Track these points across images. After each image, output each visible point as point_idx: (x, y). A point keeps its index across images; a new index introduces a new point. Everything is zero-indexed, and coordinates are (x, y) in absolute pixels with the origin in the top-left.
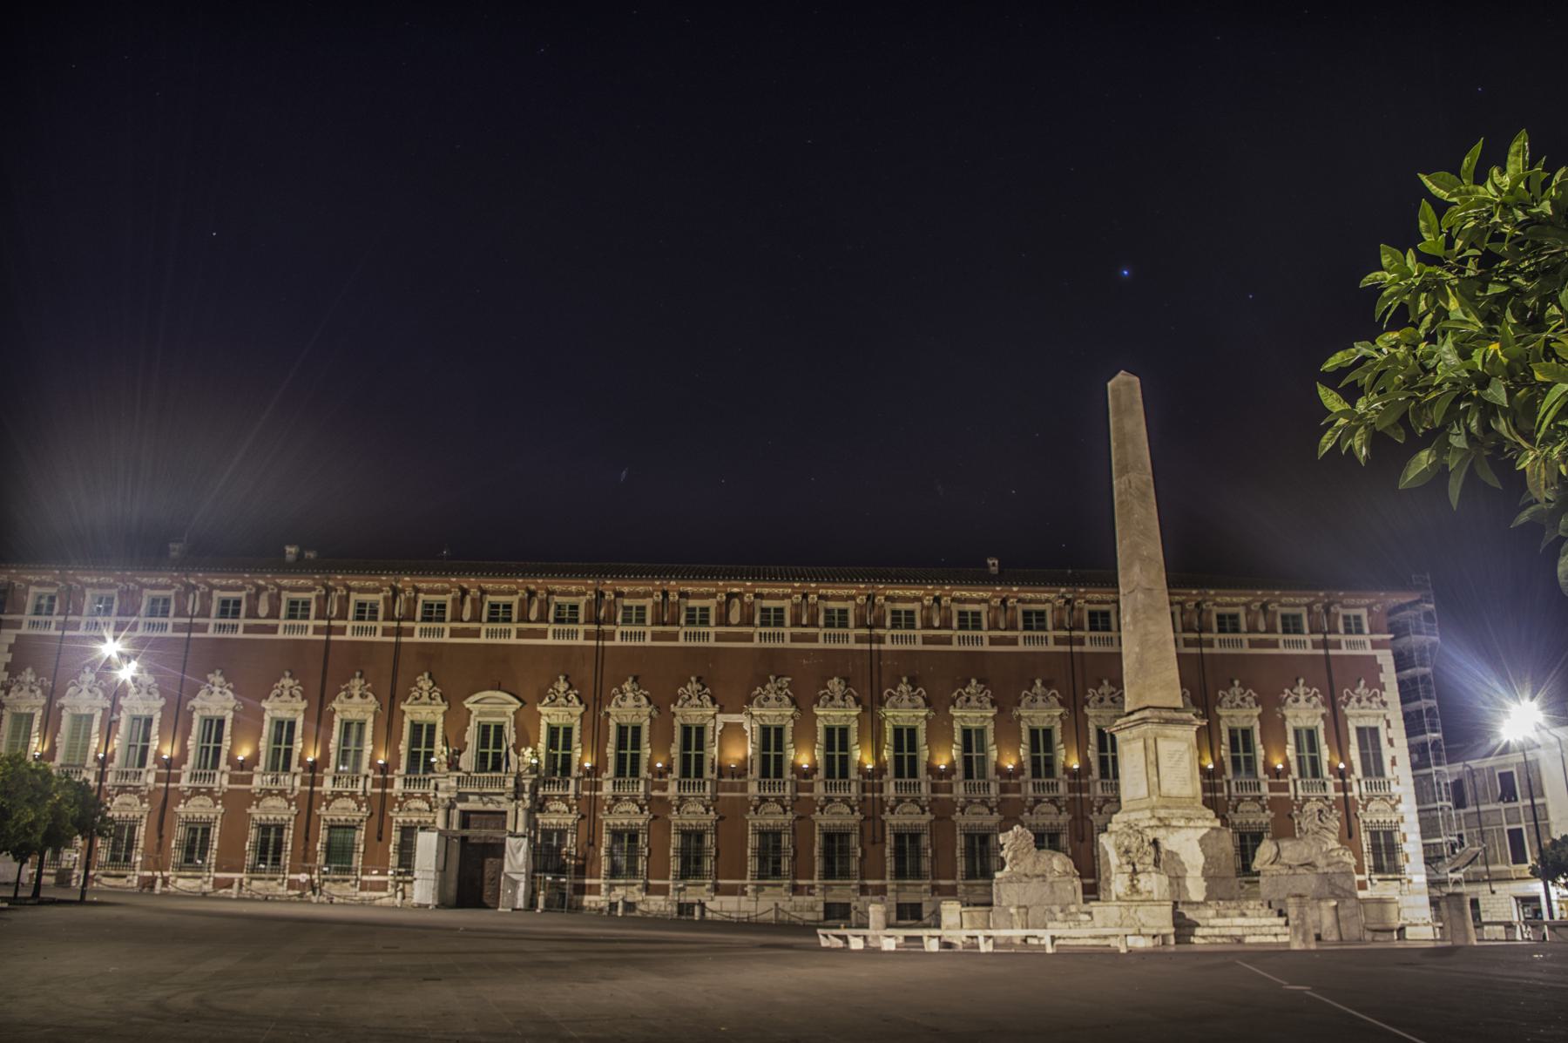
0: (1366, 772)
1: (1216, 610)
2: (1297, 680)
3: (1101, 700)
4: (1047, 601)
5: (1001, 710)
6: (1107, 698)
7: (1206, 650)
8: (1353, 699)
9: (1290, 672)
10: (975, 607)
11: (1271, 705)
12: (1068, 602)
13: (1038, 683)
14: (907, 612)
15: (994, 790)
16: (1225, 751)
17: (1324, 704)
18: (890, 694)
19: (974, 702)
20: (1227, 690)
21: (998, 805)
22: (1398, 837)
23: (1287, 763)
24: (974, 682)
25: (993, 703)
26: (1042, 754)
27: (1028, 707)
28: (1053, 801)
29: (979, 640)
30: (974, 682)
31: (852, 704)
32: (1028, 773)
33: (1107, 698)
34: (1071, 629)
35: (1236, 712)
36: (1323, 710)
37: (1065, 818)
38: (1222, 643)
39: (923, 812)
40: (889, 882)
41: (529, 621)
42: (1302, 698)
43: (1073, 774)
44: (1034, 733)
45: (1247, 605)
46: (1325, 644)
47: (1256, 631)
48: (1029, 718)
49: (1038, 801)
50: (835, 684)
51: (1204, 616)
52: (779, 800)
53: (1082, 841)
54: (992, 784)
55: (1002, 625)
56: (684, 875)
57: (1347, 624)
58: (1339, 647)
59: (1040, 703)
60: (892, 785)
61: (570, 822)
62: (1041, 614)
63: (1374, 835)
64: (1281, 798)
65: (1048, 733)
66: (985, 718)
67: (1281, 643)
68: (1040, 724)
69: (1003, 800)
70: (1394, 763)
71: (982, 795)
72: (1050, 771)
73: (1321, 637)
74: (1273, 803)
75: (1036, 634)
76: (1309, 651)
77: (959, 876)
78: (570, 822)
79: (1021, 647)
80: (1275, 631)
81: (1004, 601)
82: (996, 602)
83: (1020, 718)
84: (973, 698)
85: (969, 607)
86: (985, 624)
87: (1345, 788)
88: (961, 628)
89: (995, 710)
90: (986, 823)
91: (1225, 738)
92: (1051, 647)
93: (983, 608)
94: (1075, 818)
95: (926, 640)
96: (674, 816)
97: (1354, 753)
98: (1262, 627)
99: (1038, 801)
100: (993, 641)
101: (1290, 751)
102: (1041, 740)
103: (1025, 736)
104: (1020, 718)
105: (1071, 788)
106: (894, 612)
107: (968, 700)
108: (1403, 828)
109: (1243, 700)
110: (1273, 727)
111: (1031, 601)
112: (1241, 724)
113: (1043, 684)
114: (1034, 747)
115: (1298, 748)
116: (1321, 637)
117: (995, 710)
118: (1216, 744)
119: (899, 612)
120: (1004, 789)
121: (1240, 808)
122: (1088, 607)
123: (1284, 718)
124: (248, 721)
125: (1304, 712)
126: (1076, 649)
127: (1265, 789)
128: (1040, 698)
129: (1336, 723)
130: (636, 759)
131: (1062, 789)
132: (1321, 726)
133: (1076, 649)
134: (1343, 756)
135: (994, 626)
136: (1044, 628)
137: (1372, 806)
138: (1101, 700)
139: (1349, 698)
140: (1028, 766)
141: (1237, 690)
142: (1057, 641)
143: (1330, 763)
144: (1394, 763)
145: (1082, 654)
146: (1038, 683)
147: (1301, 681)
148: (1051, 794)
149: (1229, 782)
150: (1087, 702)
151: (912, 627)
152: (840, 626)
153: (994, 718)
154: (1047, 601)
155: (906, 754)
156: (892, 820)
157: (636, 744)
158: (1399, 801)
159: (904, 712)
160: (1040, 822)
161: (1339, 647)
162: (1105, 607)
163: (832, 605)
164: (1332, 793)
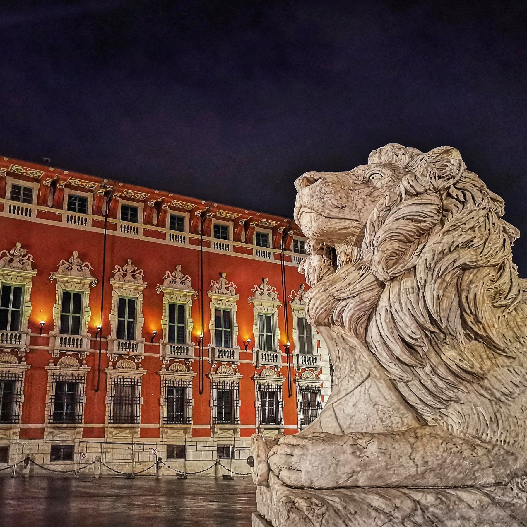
0: (302, 351)
1: (214, 221)
2: (263, 279)
3: (125, 275)
4: (90, 191)
5: (39, 273)
6: (129, 274)
7: (205, 249)
8: (298, 297)
9: (259, 272)
10: (28, 184)
11: (245, 294)
12: (107, 193)
13: (76, 254)
14: (26, 189)
15: (25, 341)
16: (212, 326)
17: (279, 299)
18: (63, 263)
19: (16, 263)
20: (216, 280)
21: (26, 356)
22: (319, 398)
23: (253, 338)
24: (19, 245)
25: (34, 266)
26: (176, 325)
27: (63, 273)
28: (76, 354)
29: (27, 212)
30: (19, 245)
31: (29, 268)
32: (57, 329)
33: (129, 274)
34: (107, 216)
35: (222, 297)
36: (278, 303)
37: (85, 370)
38: (216, 245)
39: (20, 360)
40: (47, 425)
41: (240, 241)
42: (266, 292)
43: (198, 341)
44: (66, 296)
45: (235, 221)
46: (282, 257)
47: (239, 240)
48: (64, 282)
49: (63, 354)
50: (18, 250)
51: (206, 223)
52: (76, 354)
53: (97, 391)
54: (24, 336)
55: (50, 203)
56: (57, 418)
57: (296, 246)
58: (209, 246)
59: (75, 271)
60: (116, 343)
61: (189, 379)
62: (84, 201)
63: (305, 396)
64: (247, 364)
65: (78, 297)
66: (25, 278)
67: (254, 252)
68: (73, 289)
69: (32, 351)
70: (318, 345)
71: (13, 345)
72: (182, 339)
73: (280, 252)
74: (243, 369)
75: (78, 214)
76: (272, 260)
77: (107, 421)
78: (189, 379)
79: (64, 224)
80: (165, 227)
81: (54, 183)
82: (48, 182)
83: (55, 281)
84: (16, 260)
85: (22, 183)
86: (35, 199)
87: (289, 360)
88: (12, 198)
89: (35, 272)
90: (13, 371)
91: (115, 305)
92: (89, 228)
93: (35, 186)
94: (93, 370)
95: (40, 215)
96: (51, 368)
97: (295, 335)
98: (243, 238)
99: (63, 354)
100: (40, 215)
101: (255, 330)
102: (127, 308)
103: (59, 298)
104: (55, 281)
105: (93, 345)
106: (14, 187)
107: (11, 260)
108: (322, 391)
109: (227, 288)
110: (245, 308)
111: (76, 188)
112: (128, 295)
113: (79, 256)
114: (65, 308)
115: (261, 330)
116: (280, 252)
117: (35, 272)
118: (206, 319)
119: (19, 188)
120: (33, 341)
121: (219, 370)
122: (122, 202)
123: (253, 305)
124: (154, 300)
125: (266, 303)
126: (109, 232)
127: (237, 356)
128: (75, 267)
129: (286, 312)
130: (132, 325)
131: (86, 345)
132: (276, 315)
133: (109, 232)
134: (289, 336)
135: (43, 202)
136: (84, 211)
137: (305, 375)
138: (11, 260)
139: (294, 297)
140: (58, 323)
141: (129, 267)
142: (192, 241)
143: (239, 337)
144: (318, 345)
145: (113, 237)
146: (76, 254)
147: (266, 280)
148: (75, 349)
149: (213, 349)
150: (113, 275)
151: (30, 201)
152: (25, 201)
153: (33, 279)
154: (35, 180)
155: (71, 315)
156: (112, 374)
157: (132, 313)
158: (321, 372)
159: (128, 286)
160: (63, 372)
161: (209, 246)
162: (135, 204)
163: (22, 183)
164: (280, 363)
